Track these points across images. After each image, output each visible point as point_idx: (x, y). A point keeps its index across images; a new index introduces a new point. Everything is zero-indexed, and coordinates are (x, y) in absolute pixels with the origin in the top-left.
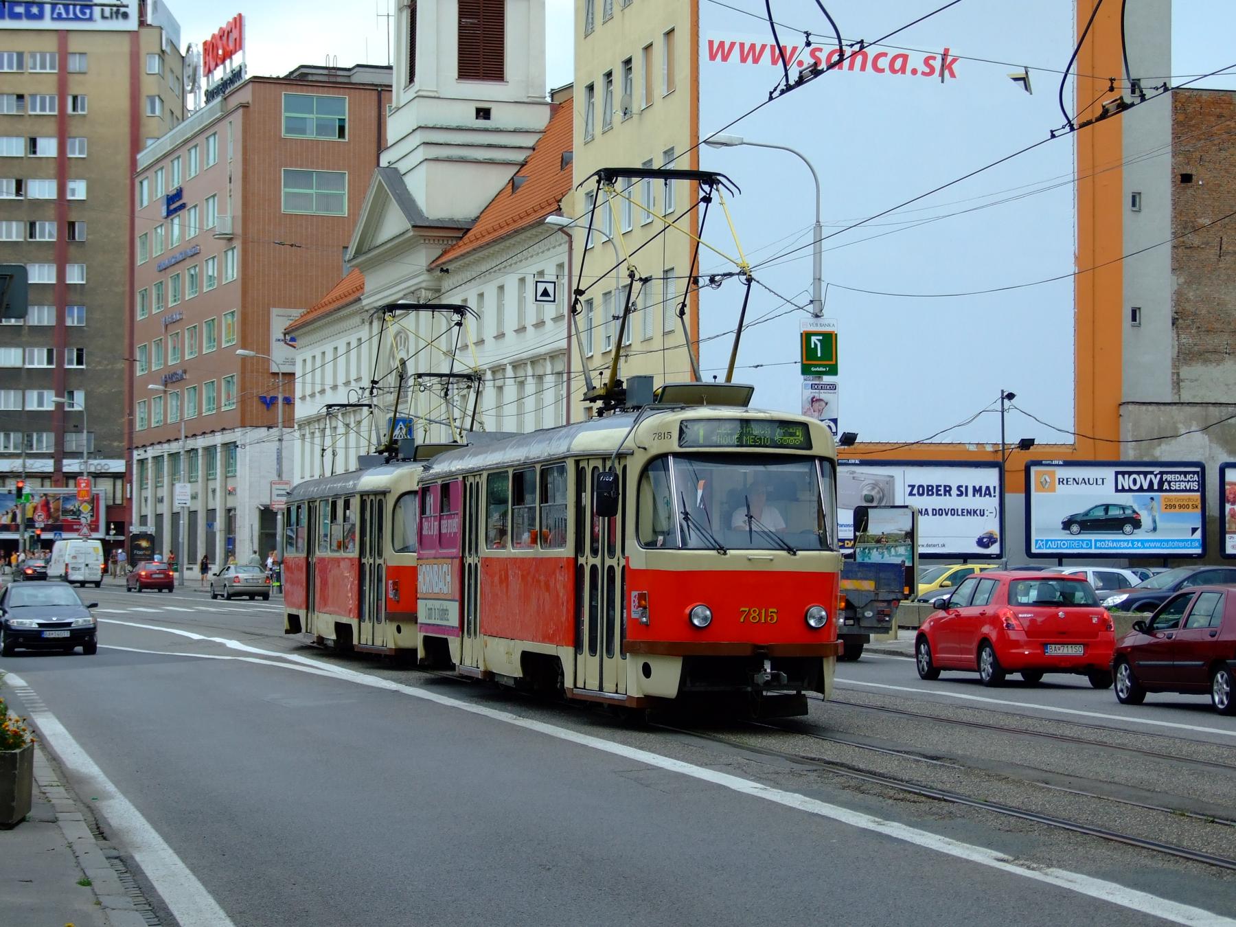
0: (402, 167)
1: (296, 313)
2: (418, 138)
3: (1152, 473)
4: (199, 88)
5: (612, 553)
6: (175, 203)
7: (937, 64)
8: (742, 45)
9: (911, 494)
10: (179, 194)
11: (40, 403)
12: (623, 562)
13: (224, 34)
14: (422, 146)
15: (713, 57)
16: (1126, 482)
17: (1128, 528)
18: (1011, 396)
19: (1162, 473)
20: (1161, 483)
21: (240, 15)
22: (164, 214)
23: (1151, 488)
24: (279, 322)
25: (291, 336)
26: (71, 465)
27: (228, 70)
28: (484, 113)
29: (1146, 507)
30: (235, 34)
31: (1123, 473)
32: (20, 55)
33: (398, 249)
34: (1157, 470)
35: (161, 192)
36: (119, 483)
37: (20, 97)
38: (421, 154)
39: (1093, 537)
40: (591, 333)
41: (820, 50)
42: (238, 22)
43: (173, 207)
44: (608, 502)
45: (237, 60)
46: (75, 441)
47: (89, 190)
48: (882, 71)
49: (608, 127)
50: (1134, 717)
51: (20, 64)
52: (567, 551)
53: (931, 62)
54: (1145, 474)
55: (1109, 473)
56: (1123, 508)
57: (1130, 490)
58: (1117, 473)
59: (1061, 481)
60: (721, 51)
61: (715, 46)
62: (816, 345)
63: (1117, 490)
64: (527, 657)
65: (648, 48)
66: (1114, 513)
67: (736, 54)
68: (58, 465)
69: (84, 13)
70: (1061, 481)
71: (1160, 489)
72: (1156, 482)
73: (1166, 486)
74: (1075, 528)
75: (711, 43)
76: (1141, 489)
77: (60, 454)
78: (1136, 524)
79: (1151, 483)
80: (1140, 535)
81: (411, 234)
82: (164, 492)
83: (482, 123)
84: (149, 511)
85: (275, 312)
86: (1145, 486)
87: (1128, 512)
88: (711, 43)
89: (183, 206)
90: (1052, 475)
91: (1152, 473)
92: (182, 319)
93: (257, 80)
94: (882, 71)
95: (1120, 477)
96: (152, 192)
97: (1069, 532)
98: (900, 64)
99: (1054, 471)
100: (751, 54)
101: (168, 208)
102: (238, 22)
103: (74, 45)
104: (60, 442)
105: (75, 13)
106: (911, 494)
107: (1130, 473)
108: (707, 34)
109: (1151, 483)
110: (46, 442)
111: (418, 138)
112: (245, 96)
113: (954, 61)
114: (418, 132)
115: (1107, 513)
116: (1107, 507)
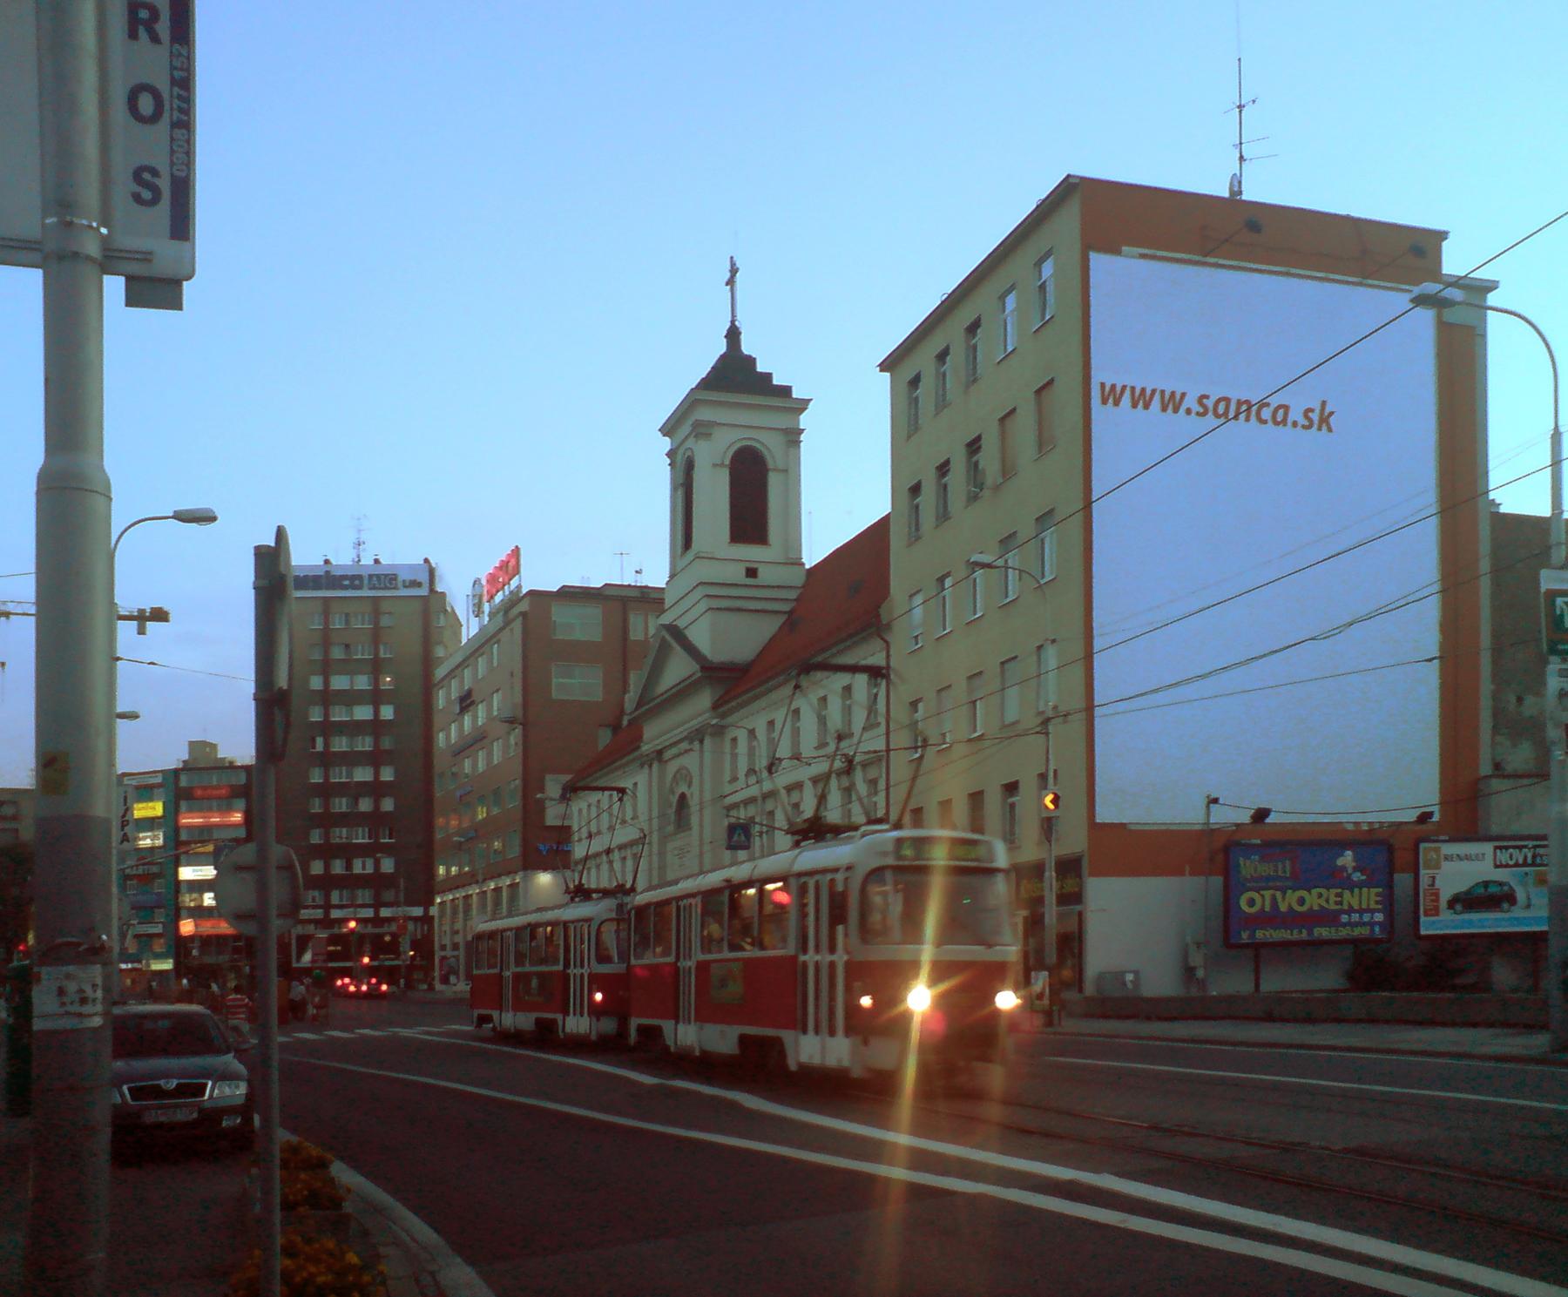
0: (681, 624)
1: (566, 778)
2: (701, 591)
3: (1525, 847)
4: (483, 612)
5: (582, 966)
6: (466, 702)
7: (1315, 416)
8: (1133, 389)
9: (1483, 854)
10: (469, 693)
11: (364, 868)
12: (589, 971)
13: (504, 566)
14: (705, 599)
15: (1105, 402)
16: (1503, 857)
17: (1505, 905)
18: (1215, 801)
19: (1535, 847)
20: (1534, 857)
21: (517, 547)
22: (458, 711)
23: (1525, 864)
24: (553, 787)
25: (571, 791)
26: (385, 912)
27: (507, 593)
28: (752, 573)
29: (1524, 884)
30: (513, 562)
31: (1500, 848)
32: (347, 615)
33: (682, 692)
34: (1531, 844)
35: (454, 695)
36: (419, 924)
37: (347, 646)
38: (703, 606)
39: (1475, 916)
40: (1003, 699)
41: (1207, 397)
42: (516, 552)
43: (464, 705)
44: (838, 914)
45: (514, 583)
46: (388, 895)
47: (396, 712)
48: (1265, 422)
49: (943, 515)
50: (1327, 1086)
51: (347, 622)
52: (560, 967)
53: (1310, 414)
54: (1520, 848)
55: (1488, 848)
56: (1501, 884)
57: (1507, 866)
58: (1496, 848)
59: (1447, 858)
60: (1112, 395)
61: (1107, 389)
62: (1562, 610)
63: (1497, 866)
64: (743, 1039)
65: (943, 469)
66: (1493, 889)
67: (1126, 400)
68: (377, 912)
69: (391, 584)
70: (1447, 858)
71: (1534, 864)
72: (1530, 856)
73: (1538, 860)
74: (1459, 907)
75: (1103, 385)
76: (1517, 865)
77: (377, 906)
78: (1511, 898)
79: (1526, 858)
80: (1517, 912)
81: (699, 674)
82: (459, 926)
83: (750, 581)
84: (447, 941)
85: (549, 778)
86: (1521, 861)
87: (1506, 888)
88: (1103, 385)
89: (473, 703)
90: (1437, 850)
91: (1525, 847)
92: (472, 791)
93: (531, 593)
94: (1265, 422)
95: (1498, 851)
96: (442, 699)
97: (1452, 911)
98: (1281, 417)
99: (1440, 848)
100: (1147, 398)
101: (461, 706)
102: (516, 552)
103: (385, 606)
104: (377, 896)
105: (385, 585)
106: (1483, 854)
107: (1507, 848)
108: (1097, 377)
109: (1526, 858)
110: (364, 895)
111: (701, 591)
112: (524, 606)
113: (1331, 413)
114: (700, 587)
115: (1486, 891)
116: (1486, 884)
